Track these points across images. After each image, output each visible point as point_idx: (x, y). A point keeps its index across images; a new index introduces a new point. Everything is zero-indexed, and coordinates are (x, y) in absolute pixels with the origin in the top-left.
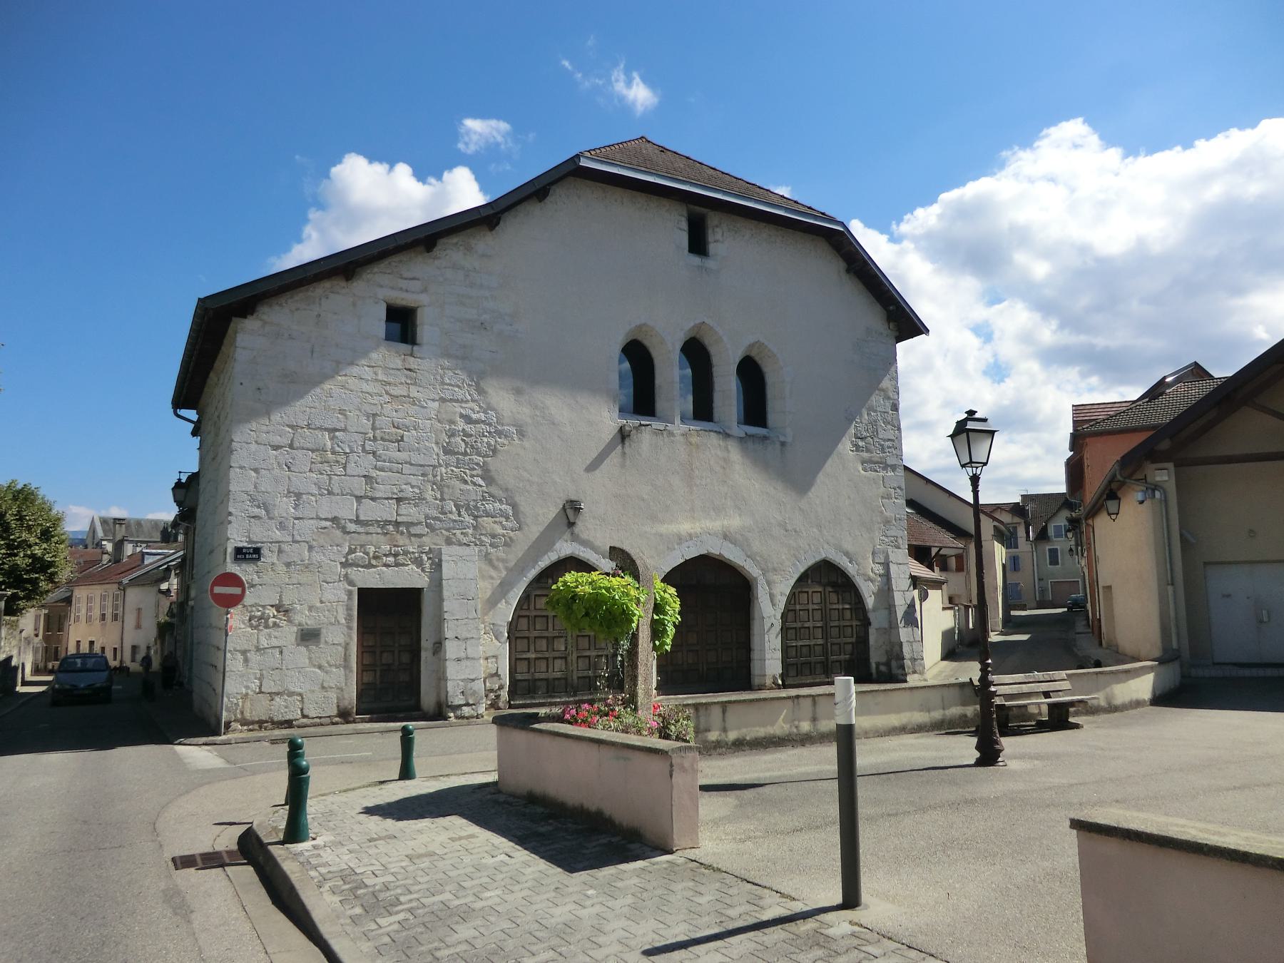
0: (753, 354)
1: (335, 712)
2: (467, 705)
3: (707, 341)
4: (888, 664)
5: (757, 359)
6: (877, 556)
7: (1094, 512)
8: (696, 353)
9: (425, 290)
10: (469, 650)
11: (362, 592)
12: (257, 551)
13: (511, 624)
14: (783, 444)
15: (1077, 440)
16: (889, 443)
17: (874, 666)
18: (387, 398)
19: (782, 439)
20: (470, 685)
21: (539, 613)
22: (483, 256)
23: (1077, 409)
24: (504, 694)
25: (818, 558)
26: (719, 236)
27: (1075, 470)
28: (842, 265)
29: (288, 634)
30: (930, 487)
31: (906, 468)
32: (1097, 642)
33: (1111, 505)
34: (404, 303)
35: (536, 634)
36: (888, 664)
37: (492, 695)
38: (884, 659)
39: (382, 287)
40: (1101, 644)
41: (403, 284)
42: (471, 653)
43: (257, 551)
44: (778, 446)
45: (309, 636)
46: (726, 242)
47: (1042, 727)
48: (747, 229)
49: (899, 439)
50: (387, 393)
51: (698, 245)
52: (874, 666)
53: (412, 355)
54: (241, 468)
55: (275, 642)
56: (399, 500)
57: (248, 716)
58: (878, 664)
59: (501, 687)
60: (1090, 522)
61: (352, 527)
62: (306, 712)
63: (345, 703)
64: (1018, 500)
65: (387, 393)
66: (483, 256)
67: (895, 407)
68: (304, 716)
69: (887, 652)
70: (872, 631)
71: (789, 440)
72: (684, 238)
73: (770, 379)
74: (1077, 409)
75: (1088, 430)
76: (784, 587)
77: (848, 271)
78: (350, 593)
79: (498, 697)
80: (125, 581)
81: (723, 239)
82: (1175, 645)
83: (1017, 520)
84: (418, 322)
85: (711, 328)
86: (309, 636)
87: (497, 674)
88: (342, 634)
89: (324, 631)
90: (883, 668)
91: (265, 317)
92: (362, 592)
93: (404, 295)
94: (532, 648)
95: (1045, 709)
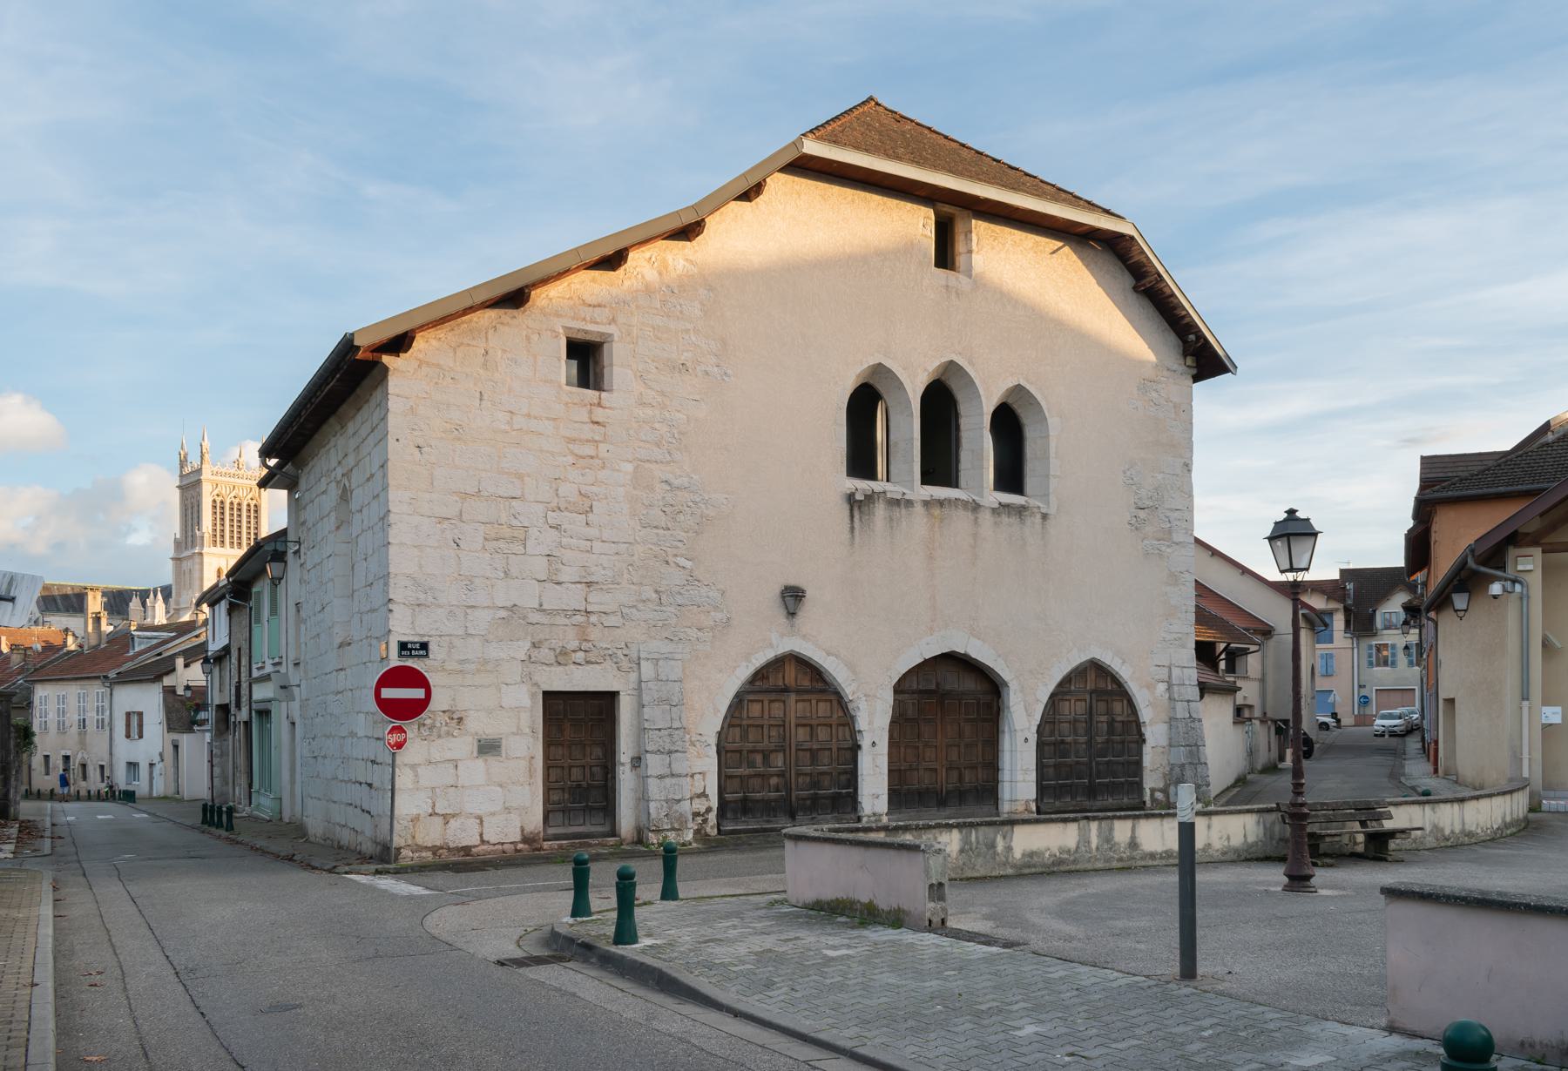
0: (1010, 401)
1: (518, 838)
2: (673, 829)
4: (1165, 791)
6: (1154, 661)
7: (1441, 602)
9: (613, 321)
11: (545, 693)
13: (720, 733)
14: (1045, 517)
15: (1425, 509)
16: (1176, 514)
17: (1148, 791)
18: (571, 459)
20: (676, 807)
23: (1428, 462)
24: (712, 817)
27: (1419, 545)
28: (1129, 281)
29: (462, 746)
30: (1216, 561)
31: (1197, 541)
32: (1431, 768)
33: (1460, 601)
35: (750, 746)
36: (1165, 791)
37: (699, 819)
38: (1161, 785)
40: (1436, 771)
42: (677, 768)
43: (424, 646)
45: (488, 747)
47: (1356, 857)
49: (1190, 509)
50: (572, 453)
52: (1148, 791)
53: (599, 405)
54: (402, 544)
55: (449, 755)
56: (589, 584)
57: (420, 841)
58: (1153, 791)
59: (709, 810)
60: (1432, 614)
61: (535, 617)
62: (486, 838)
64: (1336, 576)
65: (572, 453)
67: (1188, 467)
68: (483, 842)
69: (1165, 775)
70: (1147, 749)
71: (1052, 511)
74: (1428, 462)
75: (1446, 485)
76: (708, 719)
77: (1135, 289)
78: (533, 695)
79: (705, 821)
80: (112, 674)
82: (1526, 774)
83: (1332, 605)
84: (606, 362)
86: (488, 747)
87: (703, 795)
88: (526, 745)
89: (504, 742)
90: (1159, 795)
92: (545, 693)
95: (1360, 838)
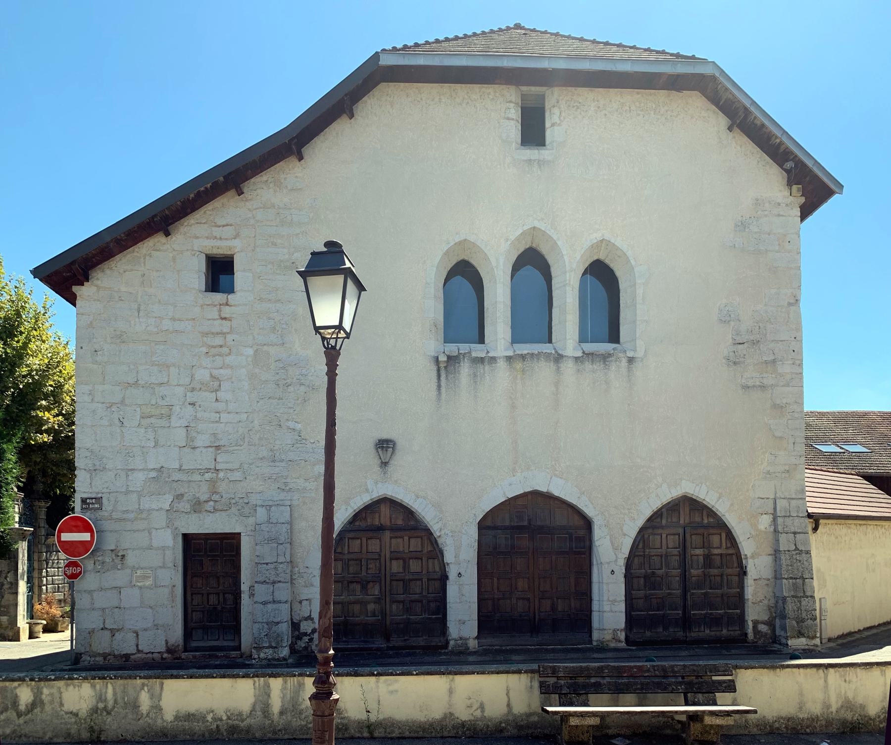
1: (163, 649)
3: (544, 250)
5: (607, 261)
8: (532, 262)
10: (276, 594)
12: (99, 500)
17: (750, 624)
19: (630, 354)
21: (352, 556)
22: (292, 190)
25: (676, 493)
26: (555, 119)
34: (220, 252)
36: (770, 623)
38: (765, 617)
39: (199, 236)
41: (217, 232)
44: (624, 363)
46: (572, 120)
48: (590, 97)
51: (533, 131)
52: (750, 624)
63: (172, 641)
66: (292, 190)
68: (139, 651)
71: (640, 354)
72: (514, 130)
73: (622, 286)
78: (175, 538)
79: (311, 640)
81: (565, 117)
85: (544, 233)
90: (763, 628)
91: (99, 282)
92: (185, 536)
93: (219, 243)
94: (221, 638)
